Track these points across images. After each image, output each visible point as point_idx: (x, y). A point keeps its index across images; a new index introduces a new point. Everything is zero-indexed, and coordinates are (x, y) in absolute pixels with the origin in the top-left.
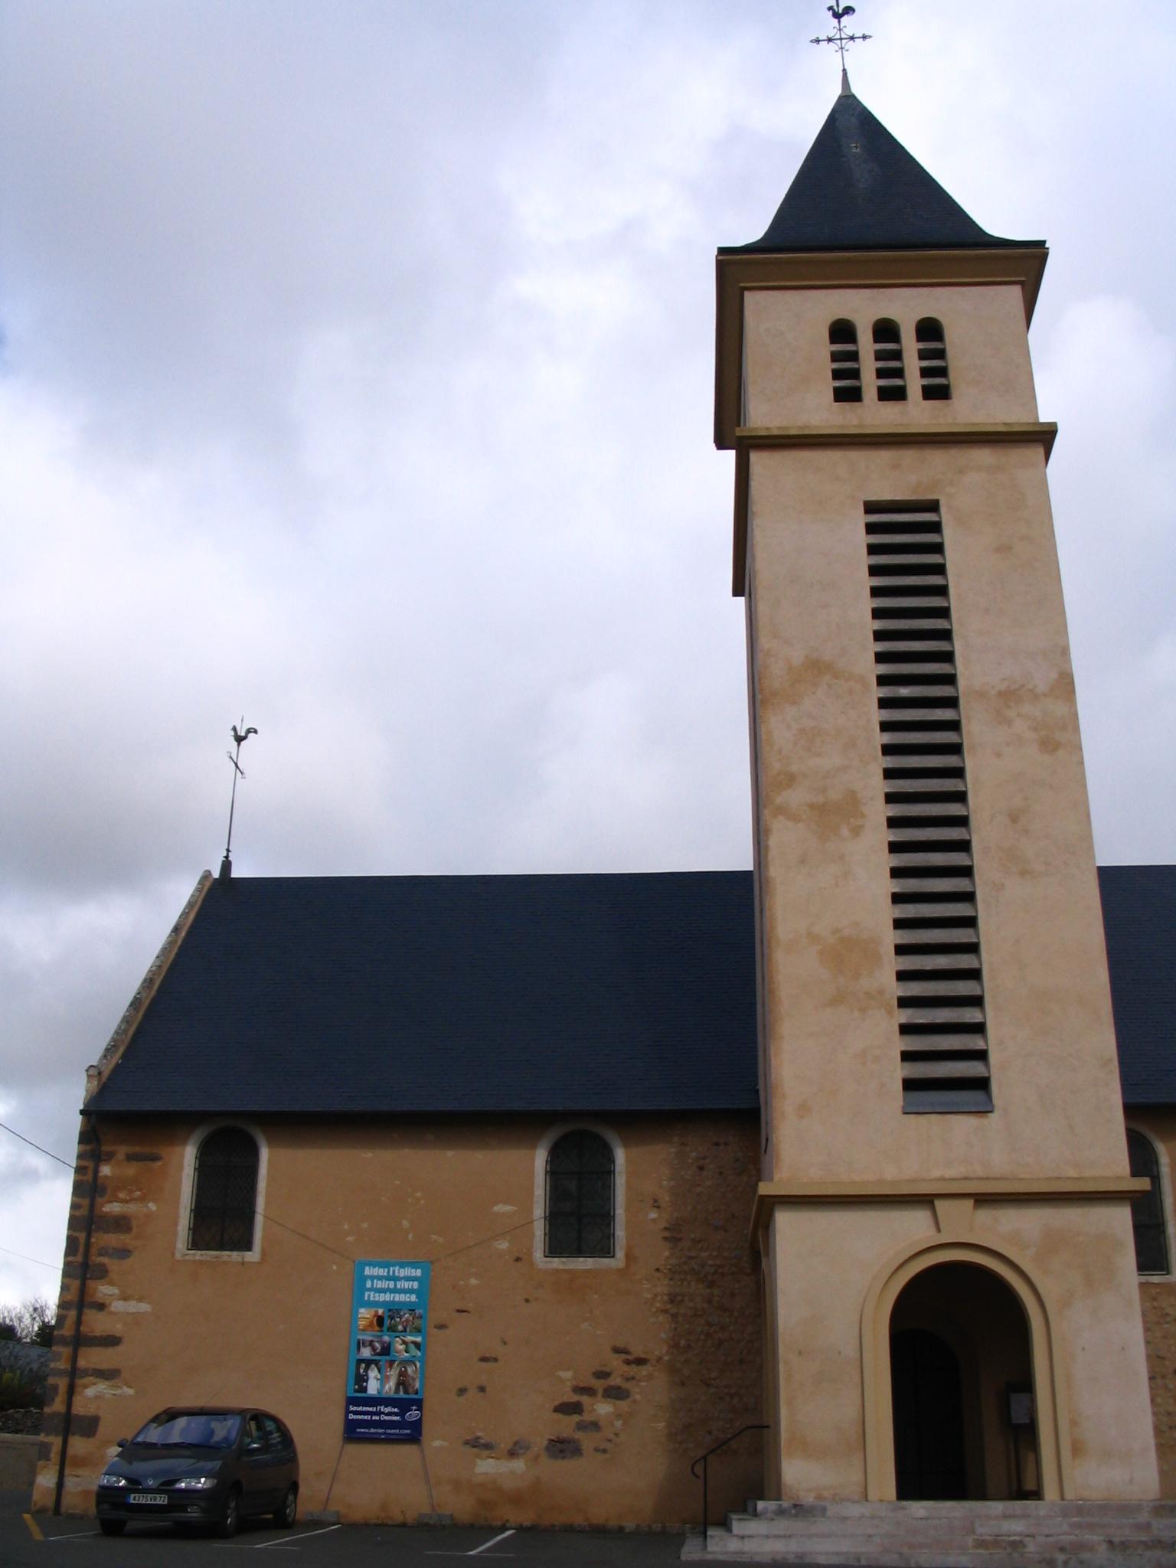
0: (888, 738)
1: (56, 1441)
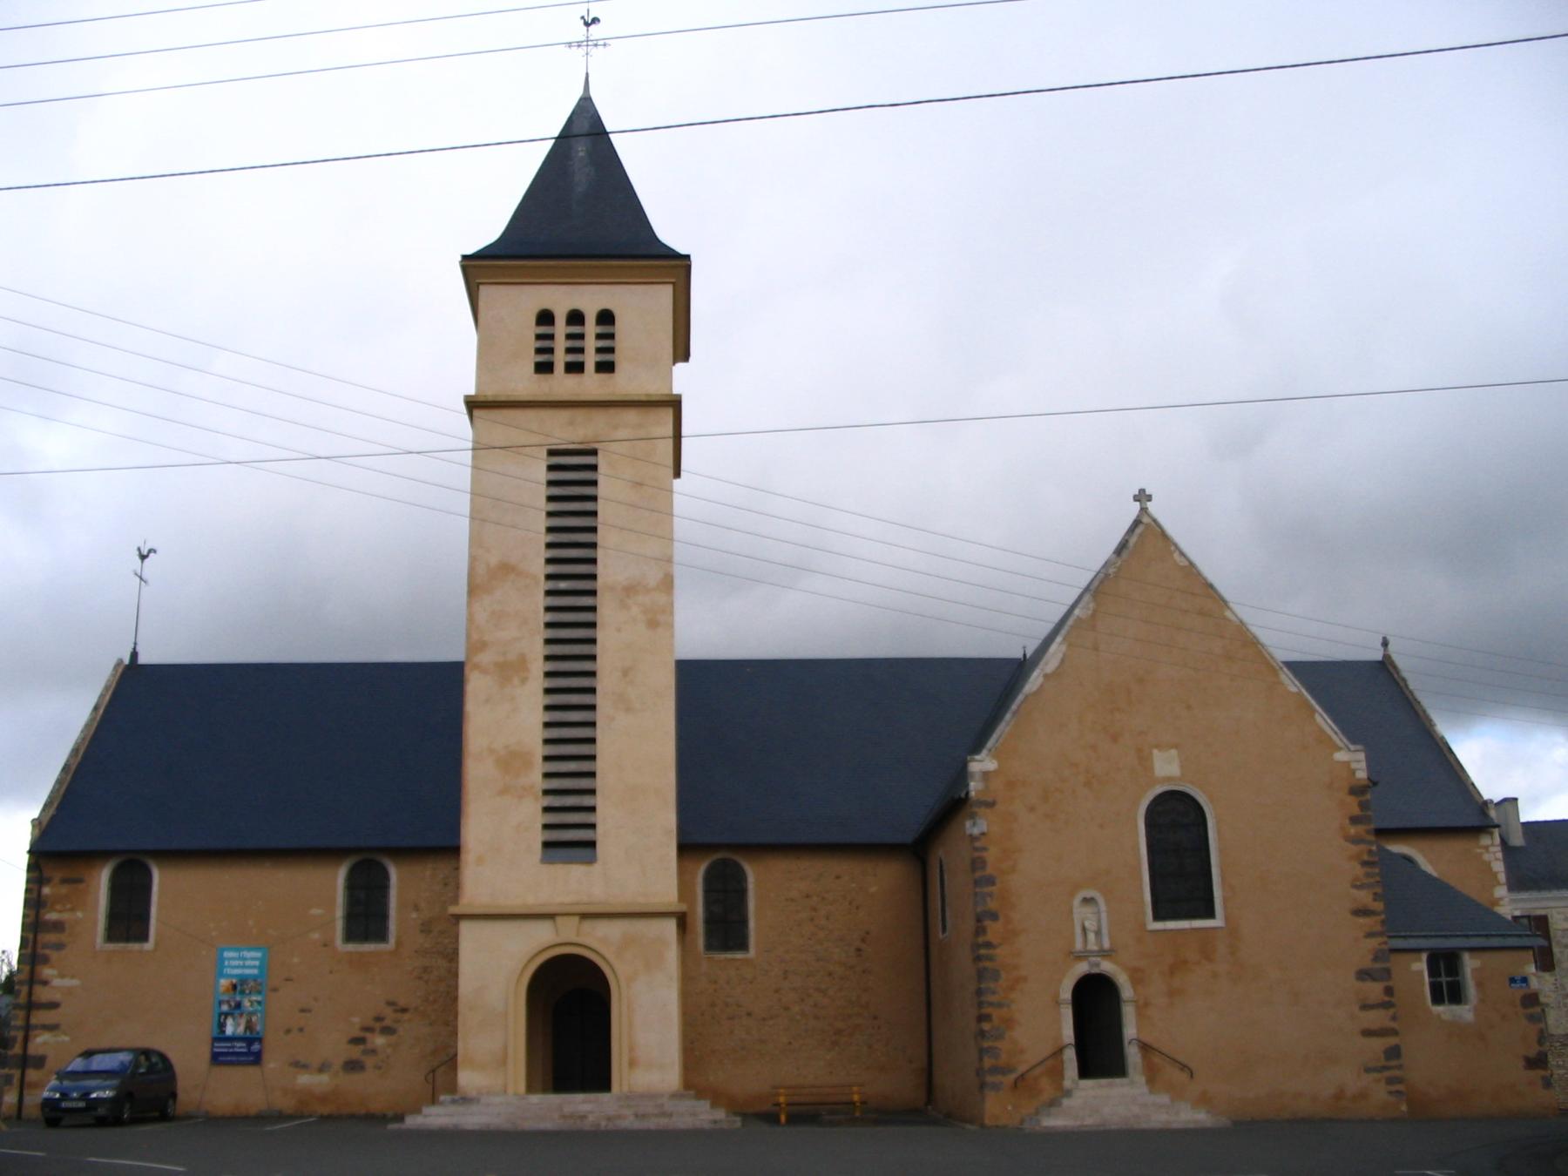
0: (550, 617)
1: (17, 1073)
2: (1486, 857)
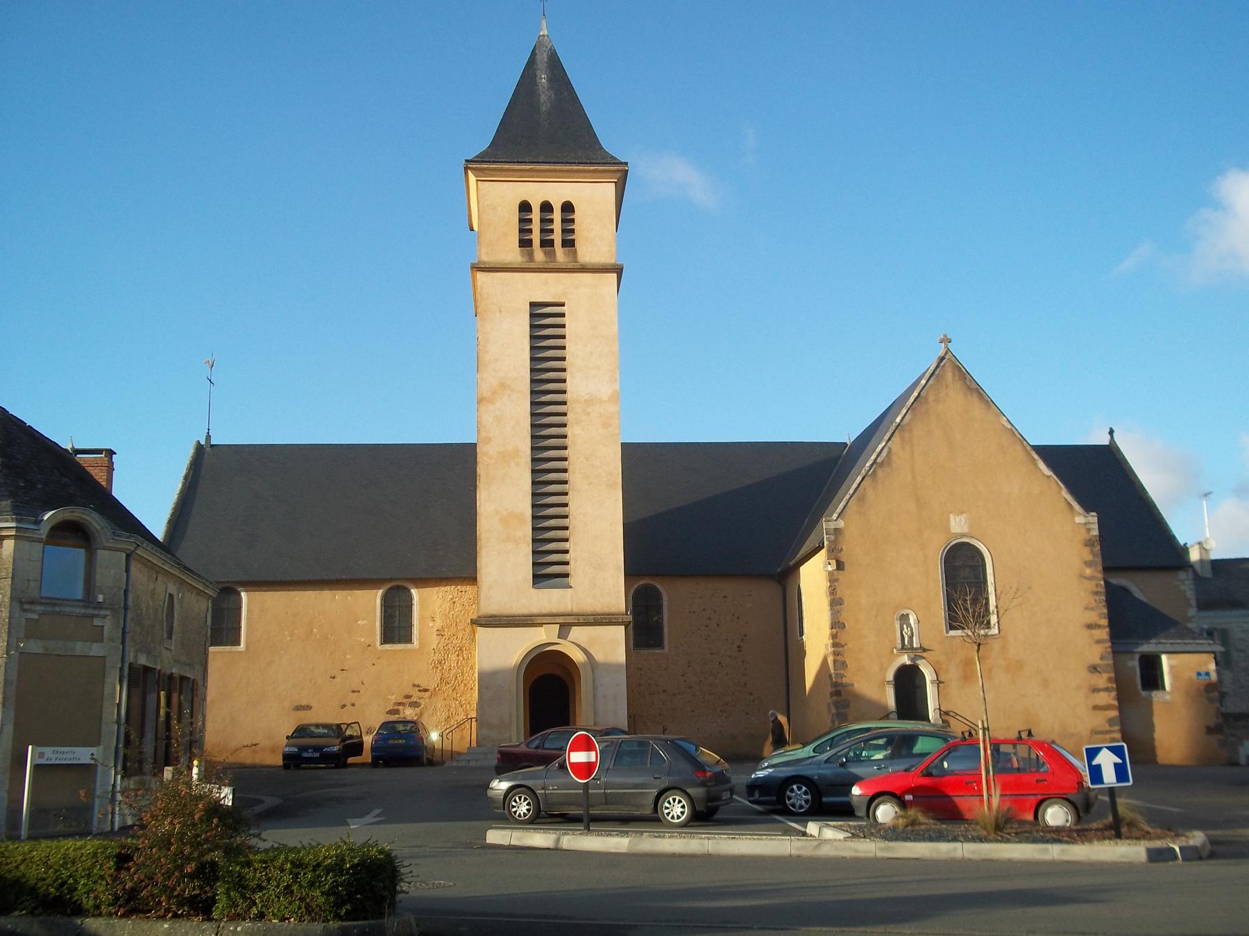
2: (1183, 588)
